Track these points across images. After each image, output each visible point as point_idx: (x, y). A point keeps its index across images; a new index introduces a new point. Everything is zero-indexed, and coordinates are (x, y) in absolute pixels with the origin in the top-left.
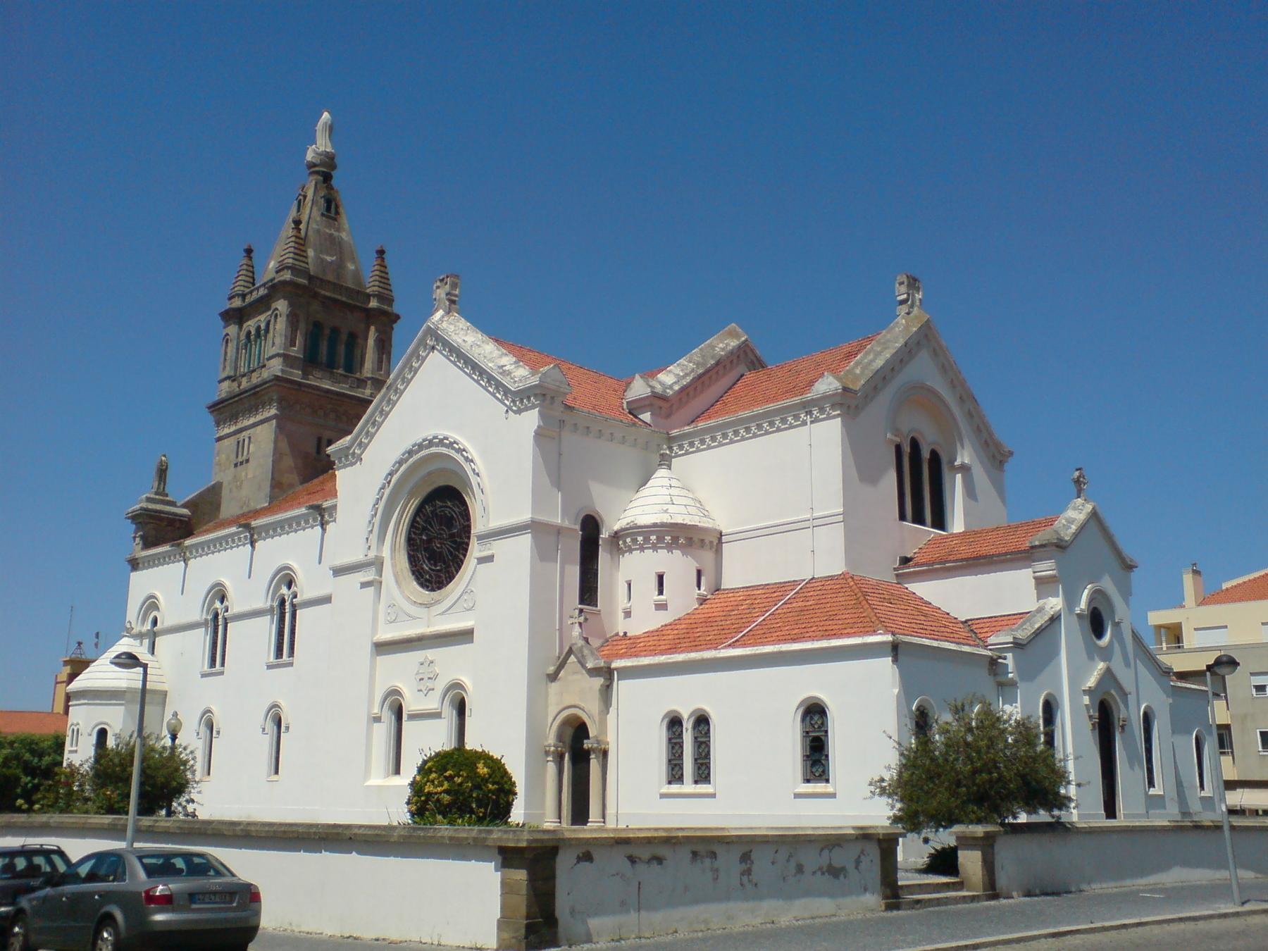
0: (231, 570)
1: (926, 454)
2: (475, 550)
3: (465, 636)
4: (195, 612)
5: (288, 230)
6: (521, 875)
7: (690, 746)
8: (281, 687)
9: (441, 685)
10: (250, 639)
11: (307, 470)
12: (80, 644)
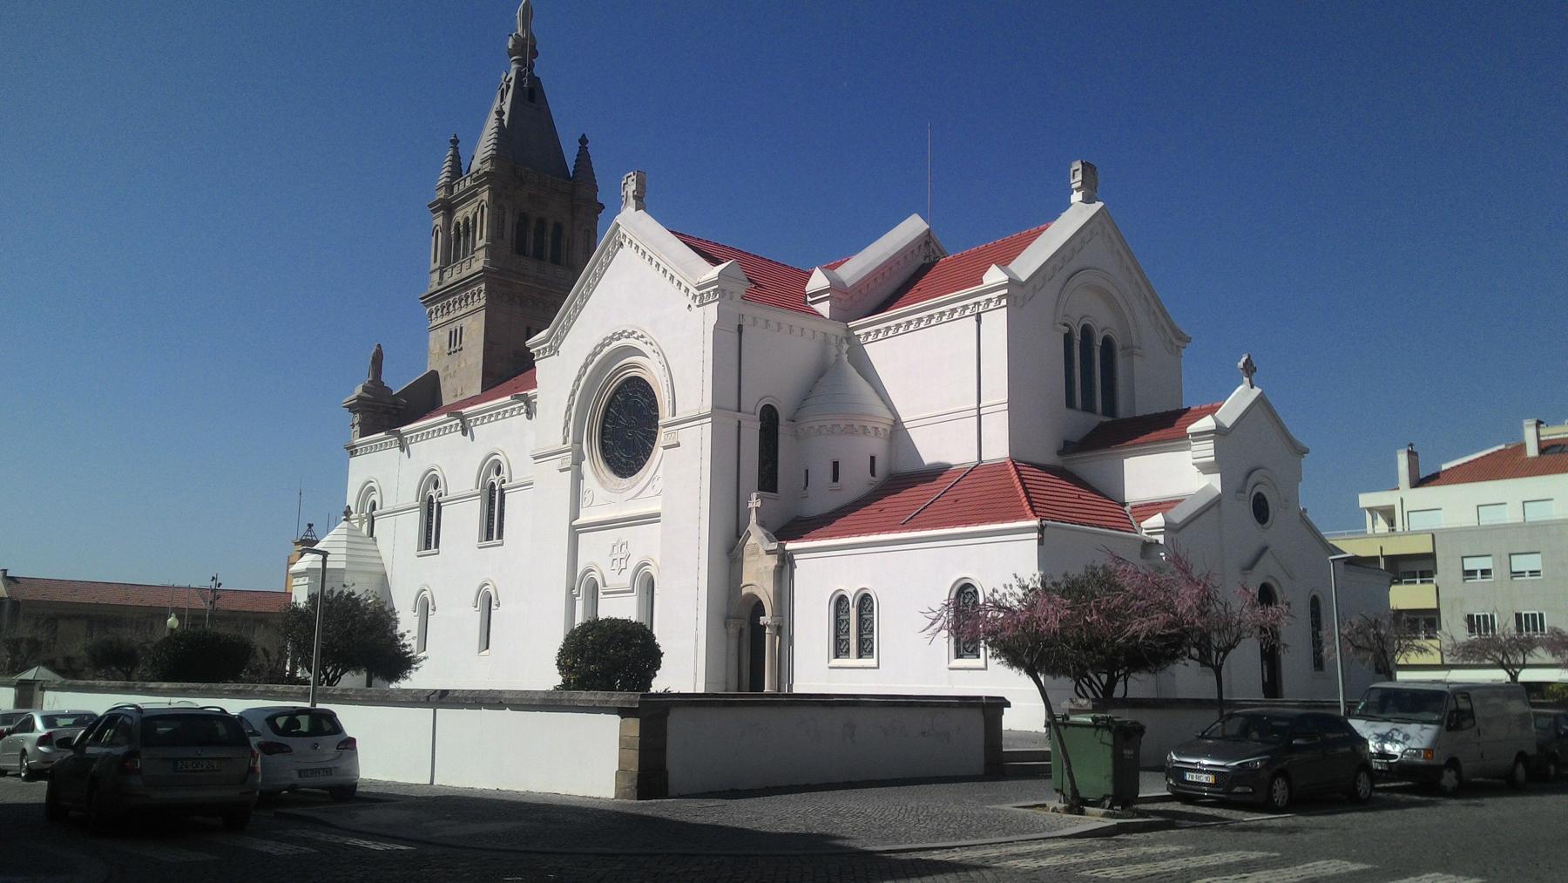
0: (444, 453)
1: (1098, 342)
2: (663, 437)
3: (653, 518)
4: (410, 497)
5: (493, 116)
6: (634, 724)
7: (855, 624)
8: (491, 564)
9: (633, 564)
10: (462, 519)
11: (508, 369)
12: (310, 526)
